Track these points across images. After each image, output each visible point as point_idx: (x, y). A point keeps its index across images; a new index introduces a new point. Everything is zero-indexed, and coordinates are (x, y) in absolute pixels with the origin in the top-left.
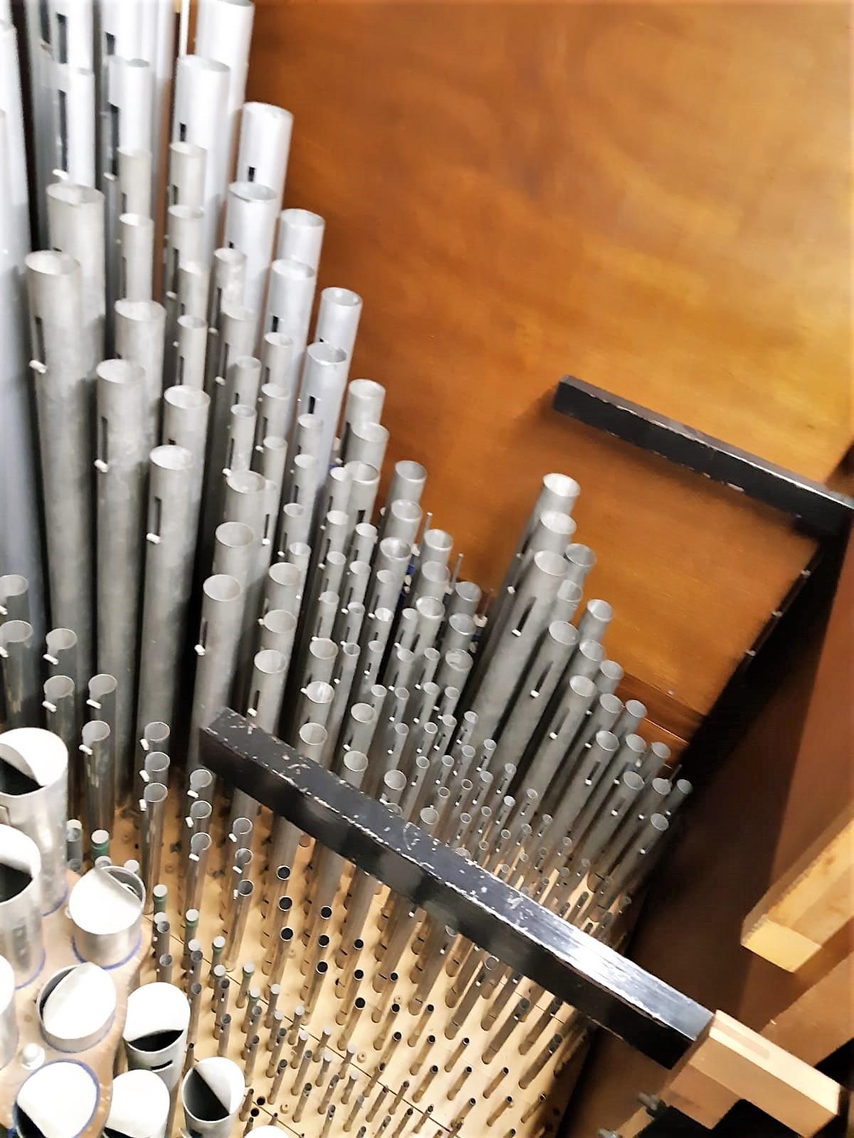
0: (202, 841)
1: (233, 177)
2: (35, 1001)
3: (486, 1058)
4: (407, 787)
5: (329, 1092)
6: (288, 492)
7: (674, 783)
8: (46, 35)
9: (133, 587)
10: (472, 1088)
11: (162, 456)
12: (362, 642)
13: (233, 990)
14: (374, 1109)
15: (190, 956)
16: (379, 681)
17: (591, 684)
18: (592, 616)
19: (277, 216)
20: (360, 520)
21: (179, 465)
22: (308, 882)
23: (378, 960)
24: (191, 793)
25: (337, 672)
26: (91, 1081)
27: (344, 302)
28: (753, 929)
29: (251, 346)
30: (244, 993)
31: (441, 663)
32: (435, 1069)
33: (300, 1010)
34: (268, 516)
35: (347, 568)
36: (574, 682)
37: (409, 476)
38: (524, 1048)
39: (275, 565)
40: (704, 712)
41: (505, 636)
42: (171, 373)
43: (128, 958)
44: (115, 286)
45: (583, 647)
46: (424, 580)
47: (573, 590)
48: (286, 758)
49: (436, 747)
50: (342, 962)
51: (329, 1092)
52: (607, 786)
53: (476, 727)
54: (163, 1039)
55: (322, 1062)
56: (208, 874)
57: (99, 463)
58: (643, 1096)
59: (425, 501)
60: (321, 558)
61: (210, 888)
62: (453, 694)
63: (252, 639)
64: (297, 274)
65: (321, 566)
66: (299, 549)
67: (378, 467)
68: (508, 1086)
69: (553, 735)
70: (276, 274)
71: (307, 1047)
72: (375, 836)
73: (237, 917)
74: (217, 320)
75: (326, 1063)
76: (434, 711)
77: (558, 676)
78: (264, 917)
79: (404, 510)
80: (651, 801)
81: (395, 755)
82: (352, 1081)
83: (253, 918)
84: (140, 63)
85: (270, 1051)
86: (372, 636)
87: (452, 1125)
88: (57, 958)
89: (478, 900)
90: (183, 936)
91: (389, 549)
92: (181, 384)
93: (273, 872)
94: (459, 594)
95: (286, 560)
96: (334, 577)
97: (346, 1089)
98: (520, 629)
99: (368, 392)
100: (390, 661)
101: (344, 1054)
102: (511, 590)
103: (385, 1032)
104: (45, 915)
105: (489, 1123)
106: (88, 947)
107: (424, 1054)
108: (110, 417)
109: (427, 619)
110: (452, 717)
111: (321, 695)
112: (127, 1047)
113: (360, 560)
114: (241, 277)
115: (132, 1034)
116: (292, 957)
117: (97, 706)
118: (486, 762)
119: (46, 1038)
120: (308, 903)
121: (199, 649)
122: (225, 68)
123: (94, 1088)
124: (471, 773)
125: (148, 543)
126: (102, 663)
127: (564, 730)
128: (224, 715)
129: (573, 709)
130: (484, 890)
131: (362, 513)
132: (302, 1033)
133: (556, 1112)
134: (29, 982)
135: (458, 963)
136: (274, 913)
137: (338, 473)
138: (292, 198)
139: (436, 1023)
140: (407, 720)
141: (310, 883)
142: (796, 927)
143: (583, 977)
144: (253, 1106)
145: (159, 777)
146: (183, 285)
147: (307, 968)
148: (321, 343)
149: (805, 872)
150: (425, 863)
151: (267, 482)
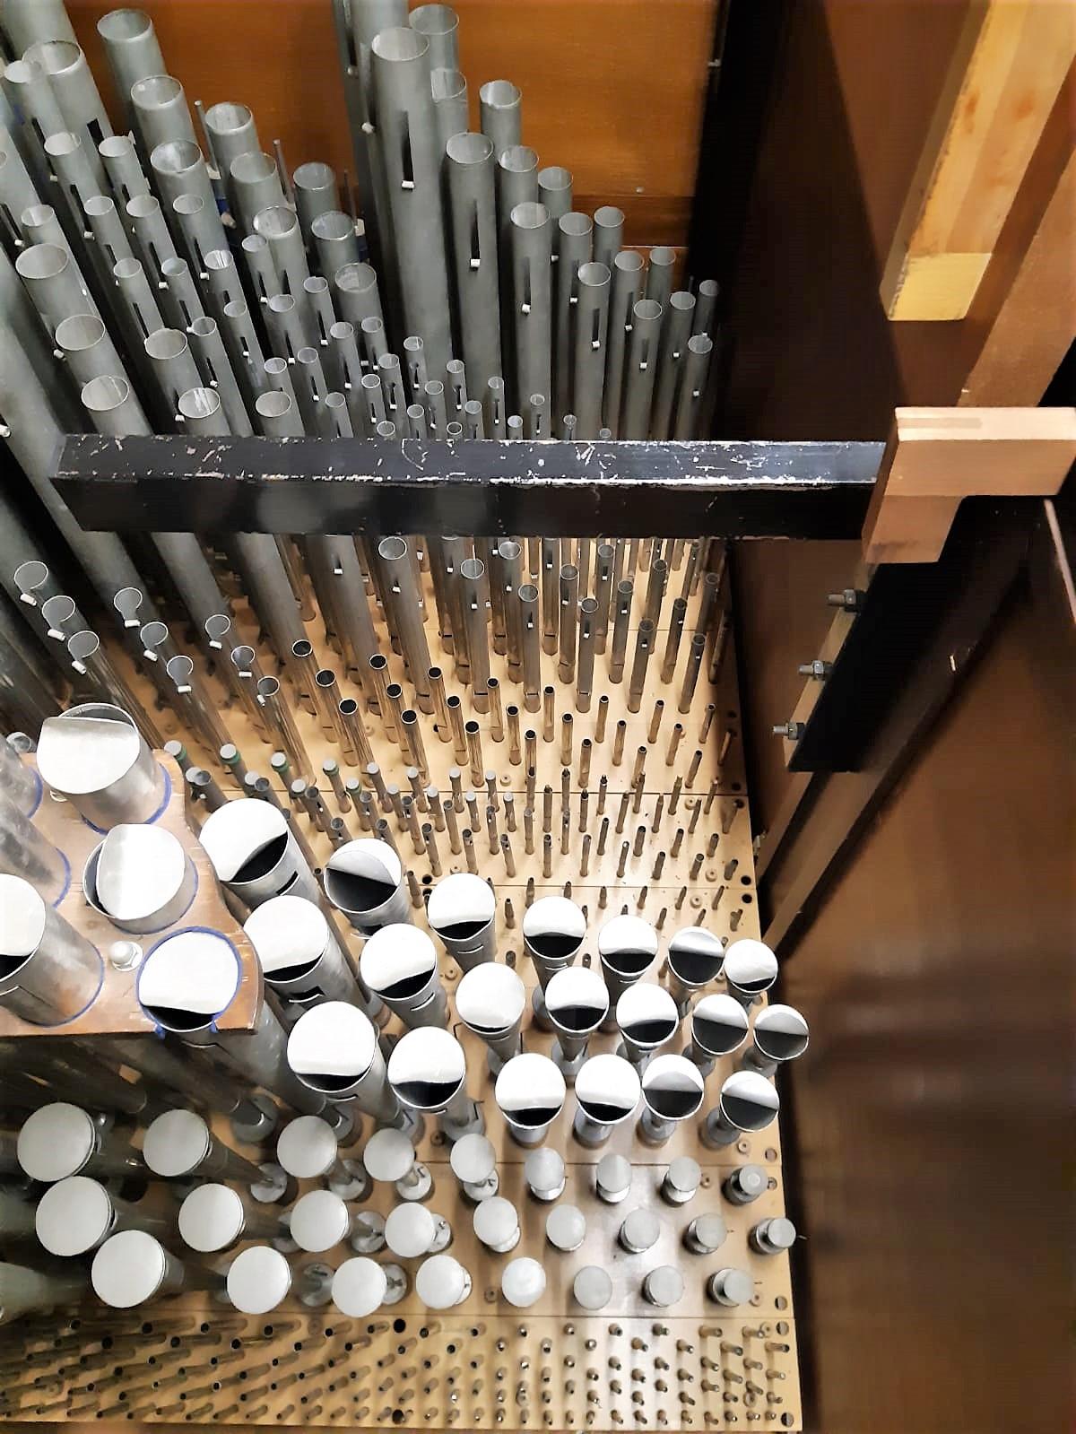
0: (179, 668)
2: (88, 904)
3: (633, 707)
5: (492, 827)
7: (696, 292)
10: (636, 736)
13: (329, 799)
14: (547, 816)
15: (256, 791)
16: (268, 354)
17: (539, 206)
18: (492, 108)
20: (98, 137)
22: (340, 654)
23: (466, 684)
24: (128, 624)
26: (213, 938)
28: (899, 286)
30: (342, 794)
31: (336, 295)
32: (587, 742)
33: (412, 772)
36: (517, 217)
37: (129, 38)
38: (666, 678)
40: (689, 191)
41: (396, 198)
43: (166, 799)
45: (503, 163)
46: (243, 186)
47: (449, 81)
48: (191, 451)
49: (392, 406)
50: (429, 706)
51: (492, 827)
52: (619, 340)
53: (426, 354)
54: (269, 855)
55: (466, 805)
56: (220, 709)
58: (805, 669)
61: (233, 720)
62: (373, 325)
68: (670, 717)
69: (526, 308)
71: (443, 798)
72: (370, 478)
73: (280, 725)
75: (472, 804)
77: (492, 217)
78: (315, 714)
79: (153, 93)
80: (680, 325)
82: (509, 804)
83: (302, 721)
85: (407, 830)
86: (221, 299)
87: (633, 787)
88: (79, 844)
89: (539, 478)
90: (236, 782)
91: (165, 163)
93: (289, 659)
94: (305, 187)
95: (30, 244)
96: (113, 235)
97: (507, 815)
98: (409, 177)
101: (486, 787)
102: (367, 127)
103: (515, 742)
104: (31, 814)
105: (669, 763)
106: (104, 810)
107: (567, 738)
109: (279, 241)
110: (390, 355)
112: (232, 888)
113: (135, 196)
115: (227, 871)
116: (370, 735)
118: (463, 392)
119: (126, 929)
120: (352, 672)
123: (223, 942)
124: (452, 413)
127: (535, 294)
128: (70, 443)
129: (532, 254)
130: (541, 462)
132: (429, 791)
133: (732, 715)
134: (66, 890)
135: (554, 636)
136: (322, 704)
139: (564, 700)
141: (342, 651)
142: (953, 247)
143: (712, 490)
144: (422, 889)
145: (74, 625)
147: (395, 734)
149: (954, 115)
150: (451, 474)
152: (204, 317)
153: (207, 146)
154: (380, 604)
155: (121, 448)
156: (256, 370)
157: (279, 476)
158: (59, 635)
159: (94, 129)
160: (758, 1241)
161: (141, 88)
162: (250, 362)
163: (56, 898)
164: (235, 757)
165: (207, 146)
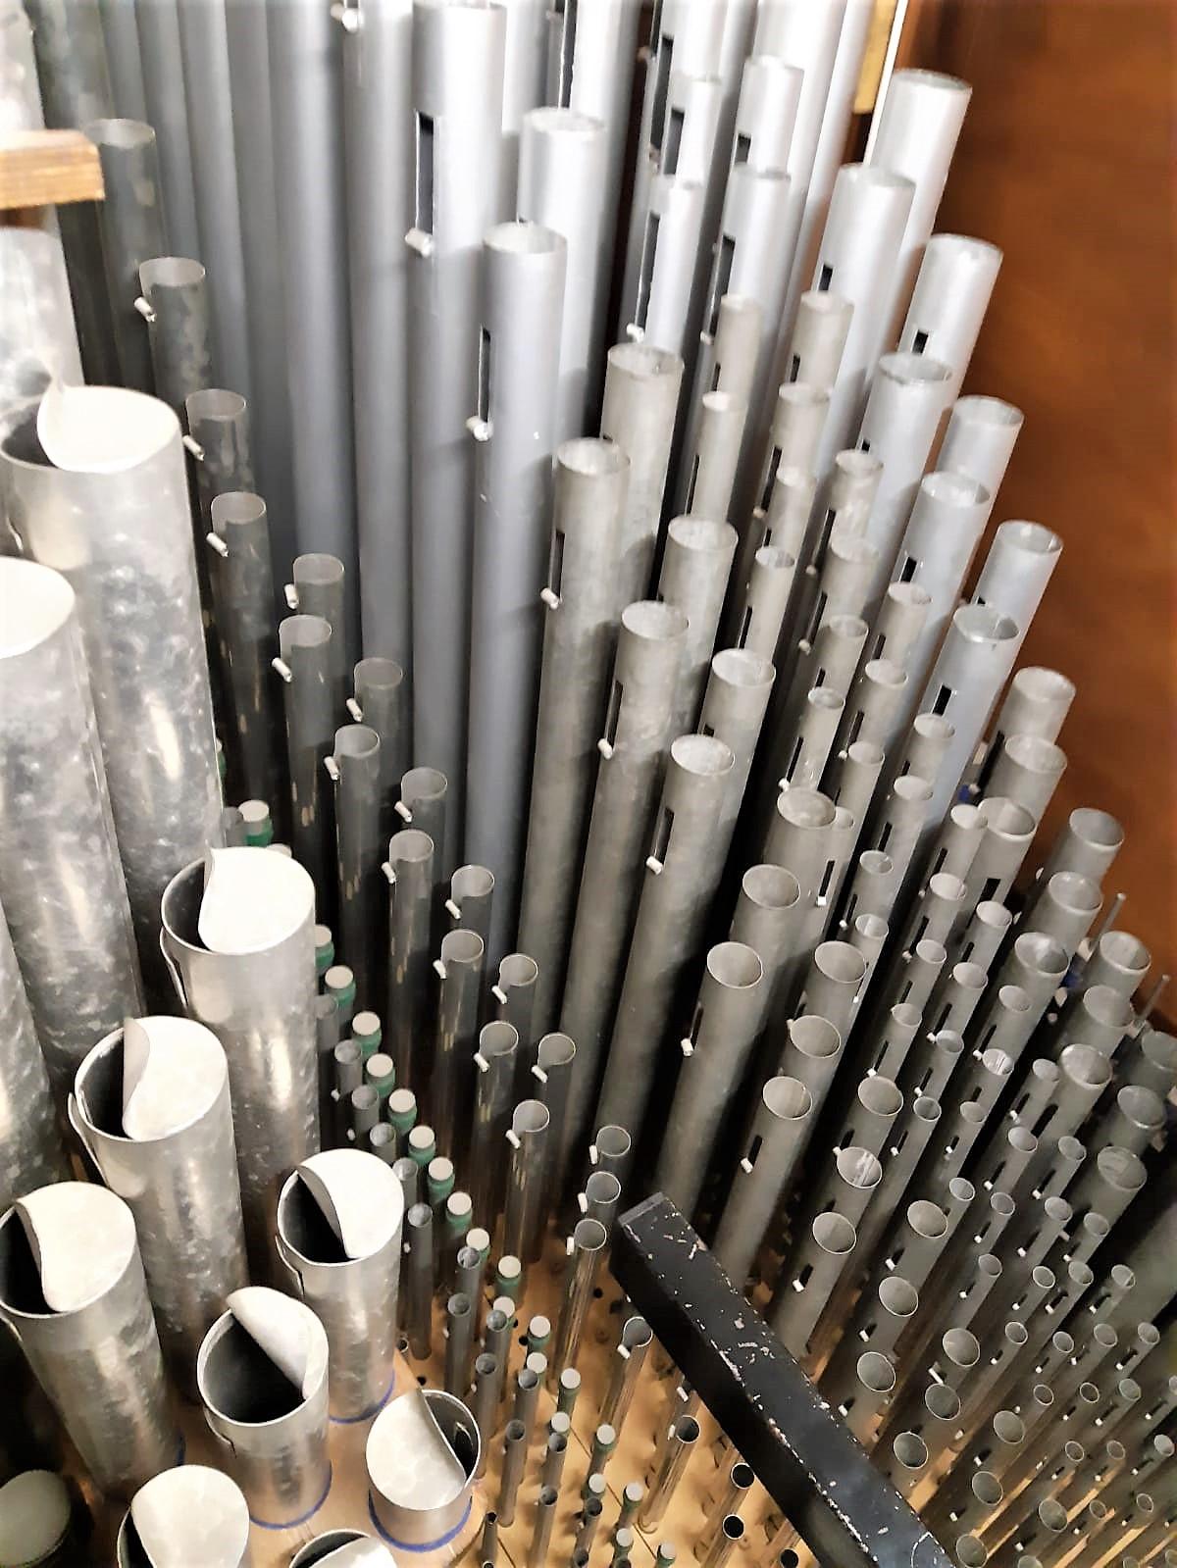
1: (893, 343)
4: (984, 1362)
6: (874, 832)
8: (657, 141)
9: (621, 924)
11: (692, 754)
12: (950, 1099)
16: (965, 1173)
19: (947, 405)
20: (987, 895)
21: (713, 767)
25: (898, 1133)
27: (1031, 548)
29: (862, 600)
31: (1087, 1167)
34: (831, 864)
35: (947, 968)
37: (1091, 835)
39: (829, 943)
42: (730, 630)
43: (439, 1543)
44: (676, 499)
46: (1084, 1015)
48: (739, 1324)
53: (1130, 1295)
57: (604, 744)
59: (1109, 883)
60: (909, 944)
62: (1096, 1226)
63: (767, 1052)
64: (959, 501)
65: (906, 955)
66: (871, 927)
67: (1038, 816)
70: (926, 496)
74: (817, 556)
76: (1060, 1240)
78: (717, 1466)
79: (1070, 890)
81: (970, 1302)
84: (779, 175)
92: (742, 647)
96: (922, 983)
99: (1046, 691)
100: (995, 1138)
108: (627, 684)
111: (862, 1169)
114: (870, 495)
117: (543, 1077)
118: (1135, 1361)
121: (687, 1045)
122: (909, 184)
124: (1100, 1375)
125: (648, 871)
126: (567, 1016)
131: (993, 884)
137: (964, 816)
138: (978, 379)
140: (1002, 1249)
146: (774, 503)
148: (980, 607)
151: (840, 813)
152: (937, 1102)
153: (1077, 973)
154: (876, 1439)
155: (691, 1256)
156: (946, 1168)
157: (783, 1436)
158: (584, 1206)
159: (993, 884)
160: (1101, 1504)
161: (1066, 877)
162: (947, 1157)
163: (284, 1522)
164: (606, 1445)
165: (1077, 973)
